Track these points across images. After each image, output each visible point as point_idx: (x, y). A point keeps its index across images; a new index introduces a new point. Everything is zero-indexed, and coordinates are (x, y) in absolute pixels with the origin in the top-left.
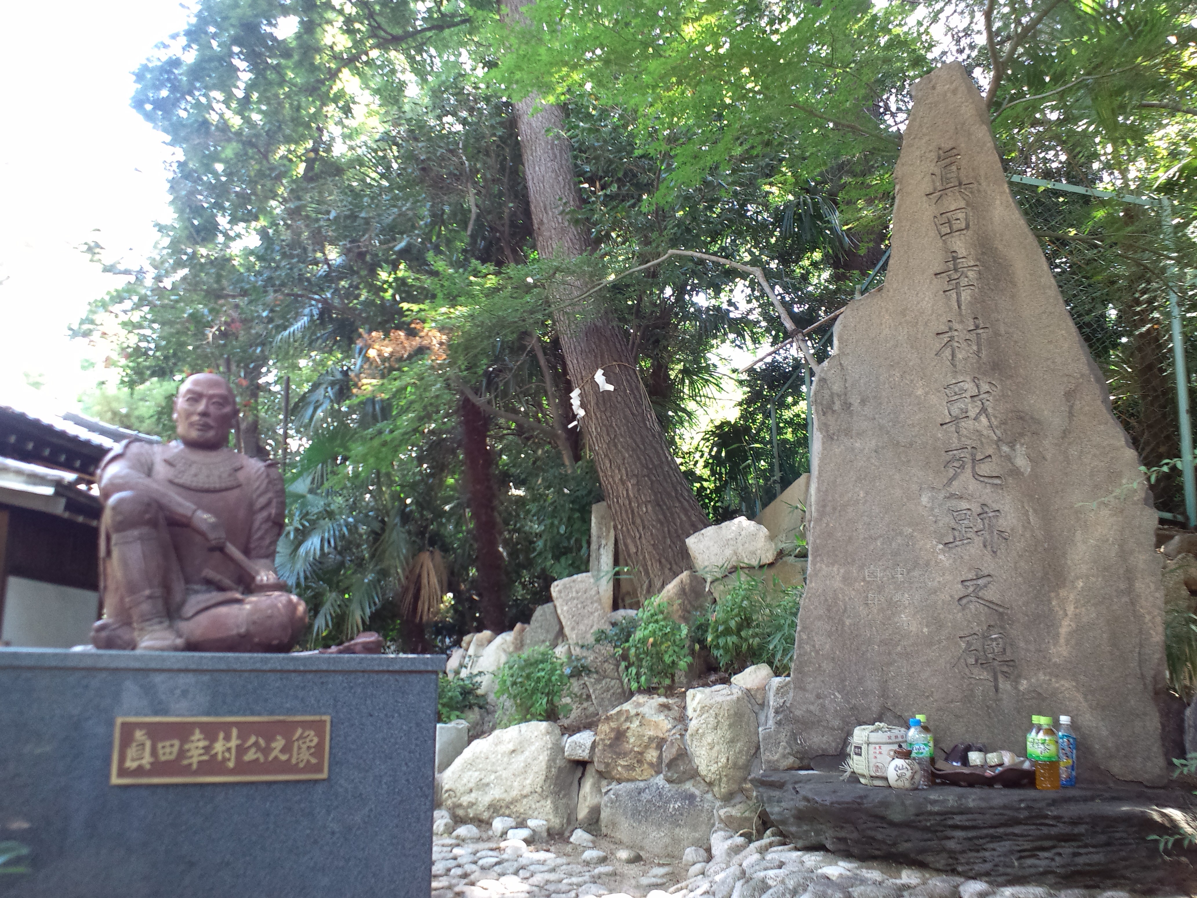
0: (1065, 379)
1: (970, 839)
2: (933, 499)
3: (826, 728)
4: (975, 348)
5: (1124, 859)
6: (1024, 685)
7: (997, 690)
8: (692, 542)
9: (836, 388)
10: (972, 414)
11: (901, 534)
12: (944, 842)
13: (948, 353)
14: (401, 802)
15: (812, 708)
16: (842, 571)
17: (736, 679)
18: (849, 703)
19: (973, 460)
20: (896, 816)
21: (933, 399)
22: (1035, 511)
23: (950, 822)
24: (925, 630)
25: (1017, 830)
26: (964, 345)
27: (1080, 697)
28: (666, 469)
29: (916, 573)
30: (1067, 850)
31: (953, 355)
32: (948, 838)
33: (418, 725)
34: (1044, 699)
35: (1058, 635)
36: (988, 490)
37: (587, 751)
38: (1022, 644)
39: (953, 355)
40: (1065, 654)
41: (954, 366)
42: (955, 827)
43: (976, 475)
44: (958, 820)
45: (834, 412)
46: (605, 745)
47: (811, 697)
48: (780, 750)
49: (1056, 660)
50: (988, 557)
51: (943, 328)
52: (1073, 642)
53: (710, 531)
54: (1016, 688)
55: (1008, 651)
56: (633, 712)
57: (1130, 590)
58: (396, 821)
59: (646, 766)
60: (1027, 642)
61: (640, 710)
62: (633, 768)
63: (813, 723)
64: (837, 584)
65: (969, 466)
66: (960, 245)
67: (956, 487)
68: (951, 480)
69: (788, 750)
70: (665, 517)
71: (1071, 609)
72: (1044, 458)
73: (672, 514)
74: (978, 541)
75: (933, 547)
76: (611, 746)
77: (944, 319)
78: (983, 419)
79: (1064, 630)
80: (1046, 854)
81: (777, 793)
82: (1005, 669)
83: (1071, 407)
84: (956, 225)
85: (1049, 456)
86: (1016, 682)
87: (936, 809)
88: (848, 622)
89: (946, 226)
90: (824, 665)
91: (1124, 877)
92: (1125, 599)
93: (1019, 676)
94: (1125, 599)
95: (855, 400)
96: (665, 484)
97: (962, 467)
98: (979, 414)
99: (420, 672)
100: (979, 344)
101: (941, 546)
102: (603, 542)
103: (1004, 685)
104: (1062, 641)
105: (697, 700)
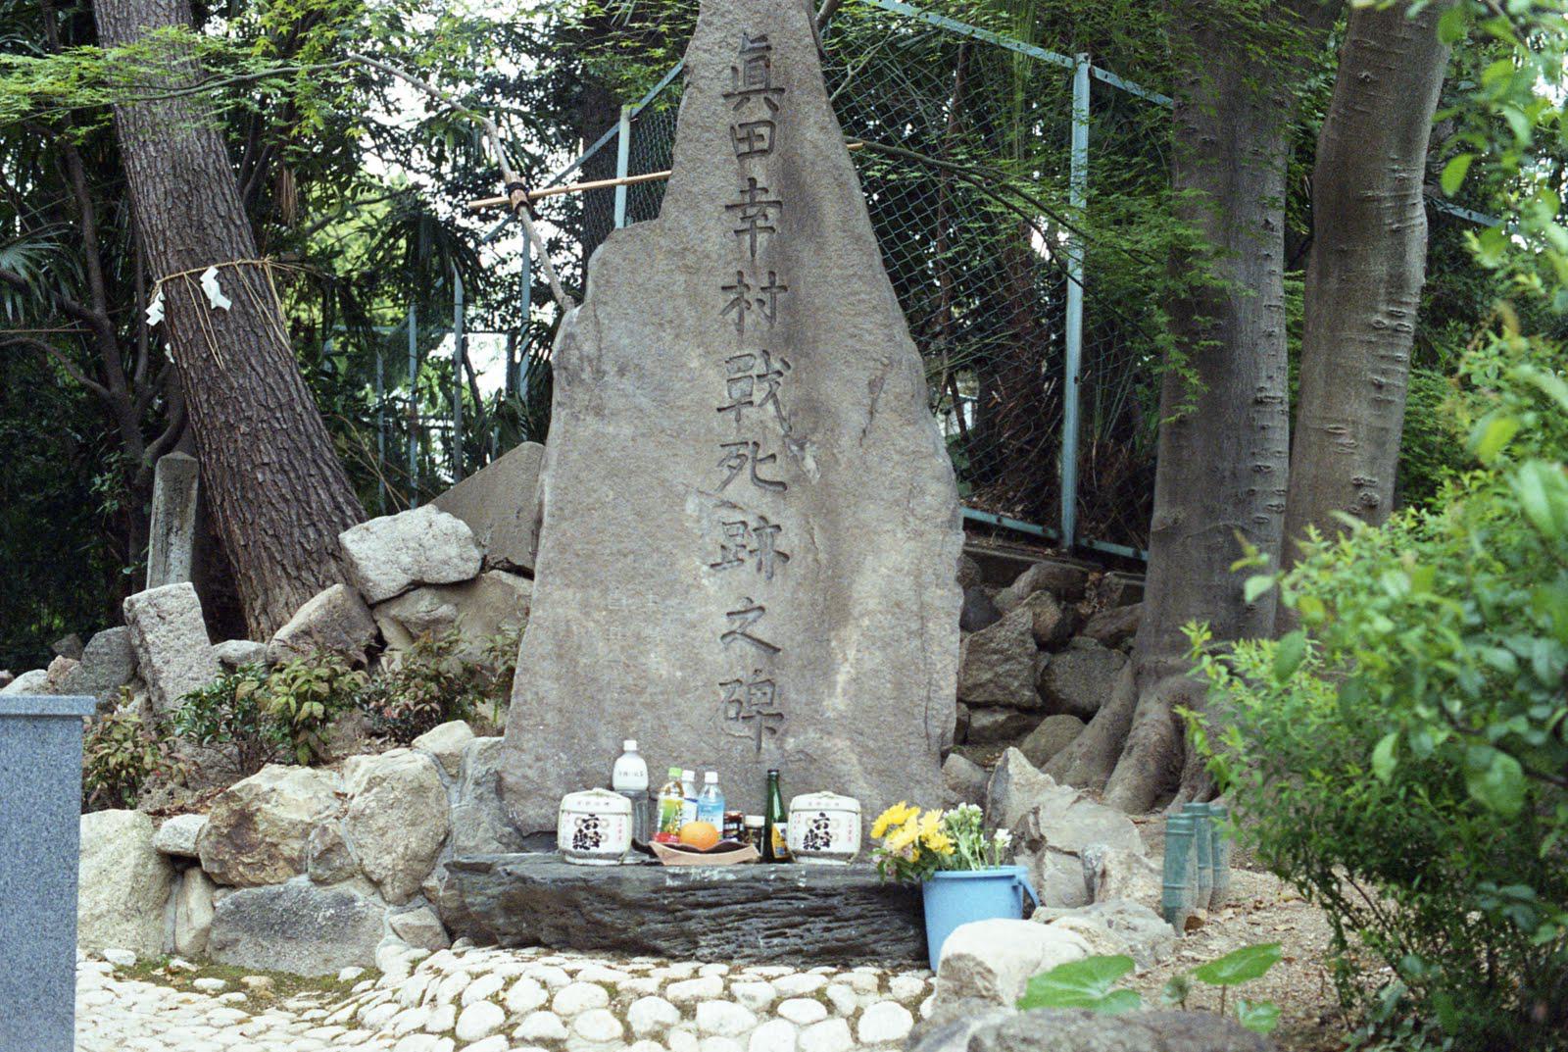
0: (871, 364)
1: (713, 918)
2: (701, 508)
3: (544, 798)
4: (768, 312)
5: (875, 932)
6: (791, 743)
7: (759, 748)
8: (348, 538)
9: (588, 348)
10: (757, 398)
11: (658, 549)
12: (686, 924)
13: (734, 314)
14: (41, 875)
15: (530, 773)
16: (579, 596)
17: (422, 740)
18: (576, 765)
19: (754, 459)
20: (630, 893)
21: (712, 374)
22: (822, 527)
23: (691, 899)
24: (679, 674)
25: (765, 905)
26: (755, 306)
27: (854, 759)
28: (299, 409)
29: (673, 602)
30: (820, 923)
31: (741, 317)
32: (688, 918)
33: (60, 782)
34: (812, 761)
35: (835, 683)
36: (768, 498)
37: (193, 840)
38: (793, 696)
39: (741, 317)
40: (842, 707)
41: (741, 331)
42: (698, 905)
43: (755, 478)
44: (701, 896)
45: (582, 381)
46: (221, 835)
47: (528, 758)
48: (480, 833)
49: (830, 714)
50: (761, 585)
51: (732, 281)
52: (852, 692)
53: (380, 523)
54: (780, 748)
55: (776, 703)
56: (266, 787)
57: (921, 633)
58: (35, 897)
59: (282, 863)
60: (798, 691)
61: (278, 785)
62: (262, 867)
63: (529, 792)
64: (574, 613)
65: (748, 466)
66: (758, 169)
67: (731, 493)
68: (726, 483)
69: (491, 834)
70: (294, 491)
71: (852, 654)
72: (837, 462)
73: (305, 490)
74: (751, 563)
75: (697, 568)
76: (228, 836)
77: (732, 270)
78: (770, 407)
79: (841, 678)
80: (795, 931)
81: (482, 879)
82: (771, 723)
83: (874, 401)
84: (759, 145)
85: (843, 460)
86: (781, 741)
87: (677, 883)
88: (583, 661)
89: (746, 141)
90: (549, 716)
91: (874, 953)
92: (916, 643)
93: (786, 733)
94: (916, 643)
95: (610, 367)
96: (294, 436)
97: (740, 467)
98: (766, 399)
99: (64, 718)
100: (773, 309)
101: (705, 568)
102: (176, 523)
103: (768, 743)
104: (839, 690)
105: (360, 771)
